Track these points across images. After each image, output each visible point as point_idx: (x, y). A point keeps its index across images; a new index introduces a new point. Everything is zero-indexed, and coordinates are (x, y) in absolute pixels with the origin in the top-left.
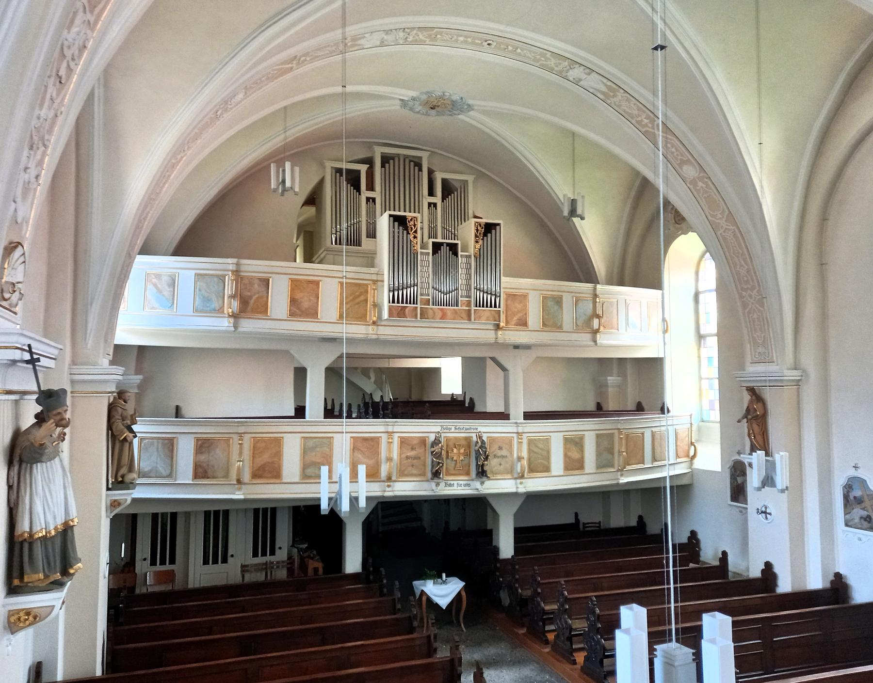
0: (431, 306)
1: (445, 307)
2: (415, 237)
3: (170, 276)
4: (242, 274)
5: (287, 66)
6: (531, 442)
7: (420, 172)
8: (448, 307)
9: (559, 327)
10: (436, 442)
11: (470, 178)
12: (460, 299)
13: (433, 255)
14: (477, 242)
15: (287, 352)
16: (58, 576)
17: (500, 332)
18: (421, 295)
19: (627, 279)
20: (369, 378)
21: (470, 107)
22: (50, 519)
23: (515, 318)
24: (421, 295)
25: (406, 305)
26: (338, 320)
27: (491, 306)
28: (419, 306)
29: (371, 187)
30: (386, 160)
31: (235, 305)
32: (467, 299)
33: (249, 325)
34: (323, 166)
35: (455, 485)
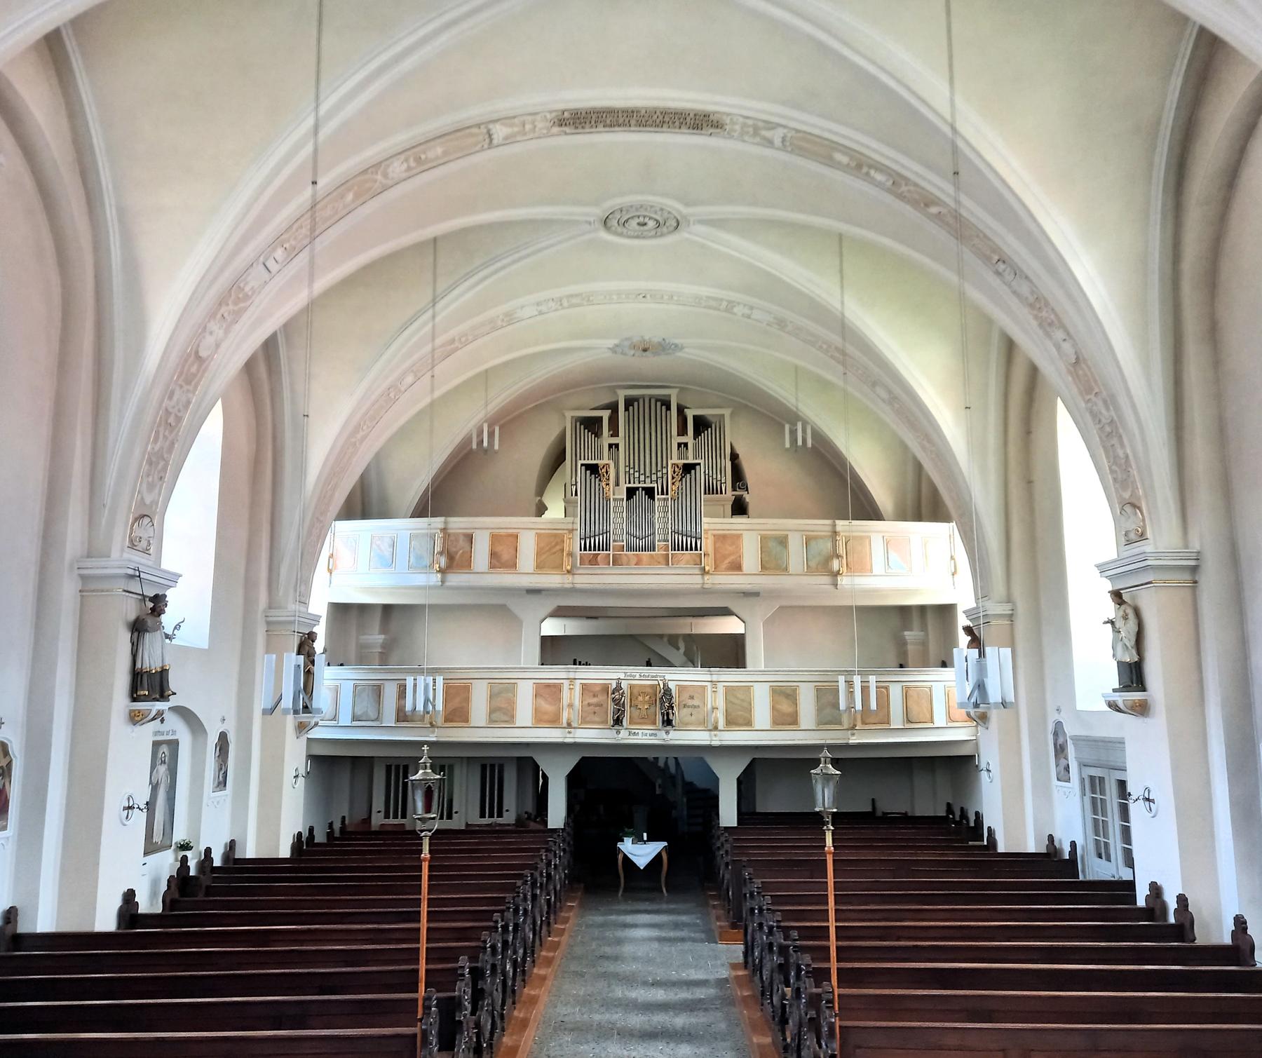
2: (608, 484)
3: (390, 537)
7: (668, 412)
10: (619, 687)
11: (727, 412)
13: (627, 500)
16: (158, 696)
17: (706, 577)
18: (614, 541)
19: (924, 510)
20: (678, 649)
21: (682, 348)
23: (727, 561)
24: (614, 541)
25: (599, 552)
27: (691, 549)
28: (611, 552)
29: (615, 433)
31: (443, 561)
33: (455, 579)
35: (640, 734)
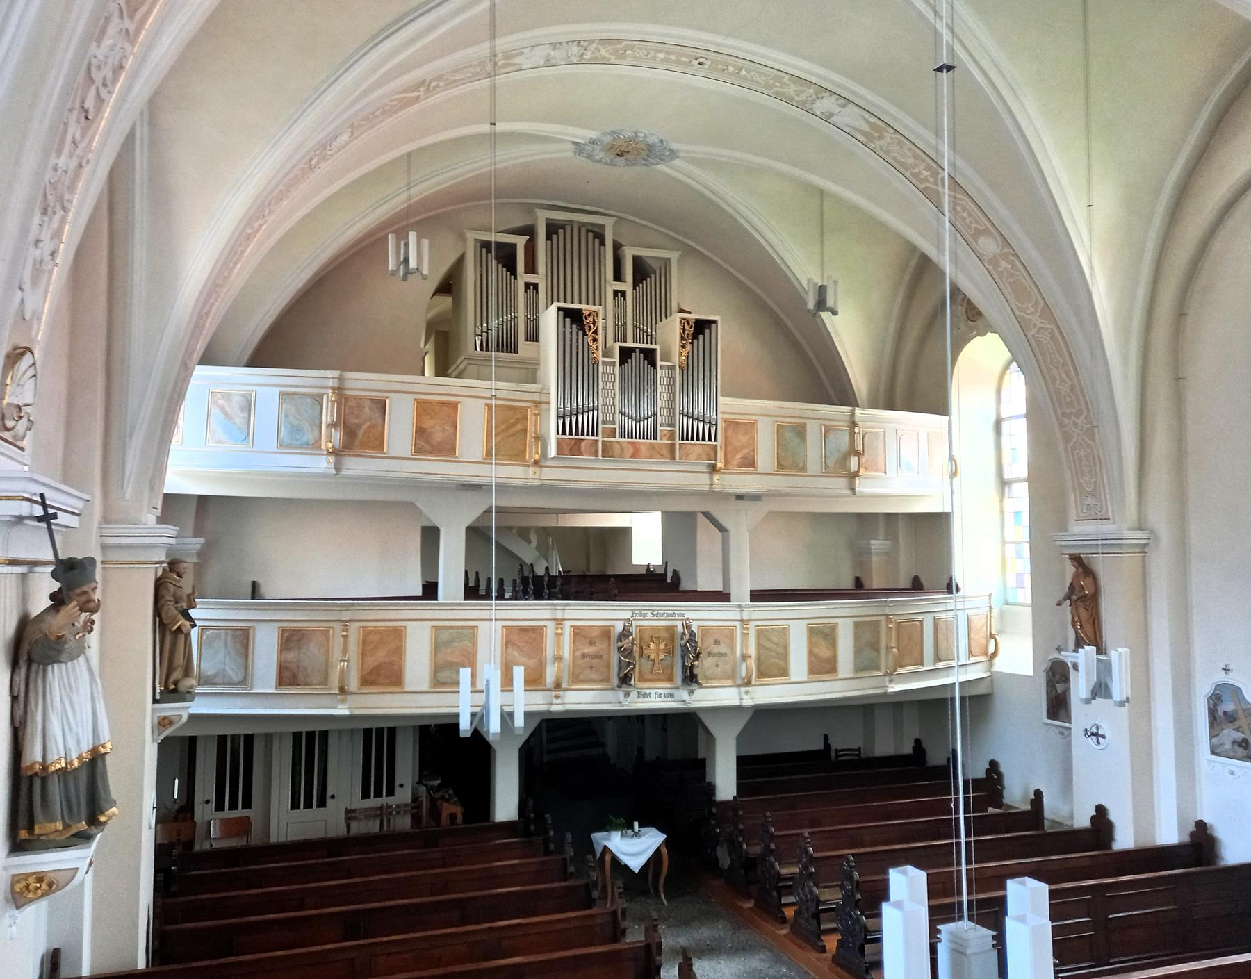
0: (617, 439)
1: (638, 440)
2: (595, 340)
3: (243, 396)
4: (347, 392)
5: (411, 95)
6: (760, 633)
7: (602, 247)
8: (642, 440)
9: (800, 469)
10: (625, 633)
11: (673, 256)
12: (659, 428)
13: (620, 365)
14: (683, 347)
15: (411, 505)
16: (83, 825)
17: (716, 477)
18: (604, 422)
19: (898, 400)
20: (529, 542)
21: (673, 154)
22: (71, 743)
23: (738, 456)
24: (604, 422)
25: (582, 437)
26: (484, 459)
27: (704, 439)
28: (600, 438)
29: (531, 268)
30: (553, 229)
31: (337, 437)
32: (669, 429)
33: (357, 466)
34: (463, 238)
35: (653, 695)
